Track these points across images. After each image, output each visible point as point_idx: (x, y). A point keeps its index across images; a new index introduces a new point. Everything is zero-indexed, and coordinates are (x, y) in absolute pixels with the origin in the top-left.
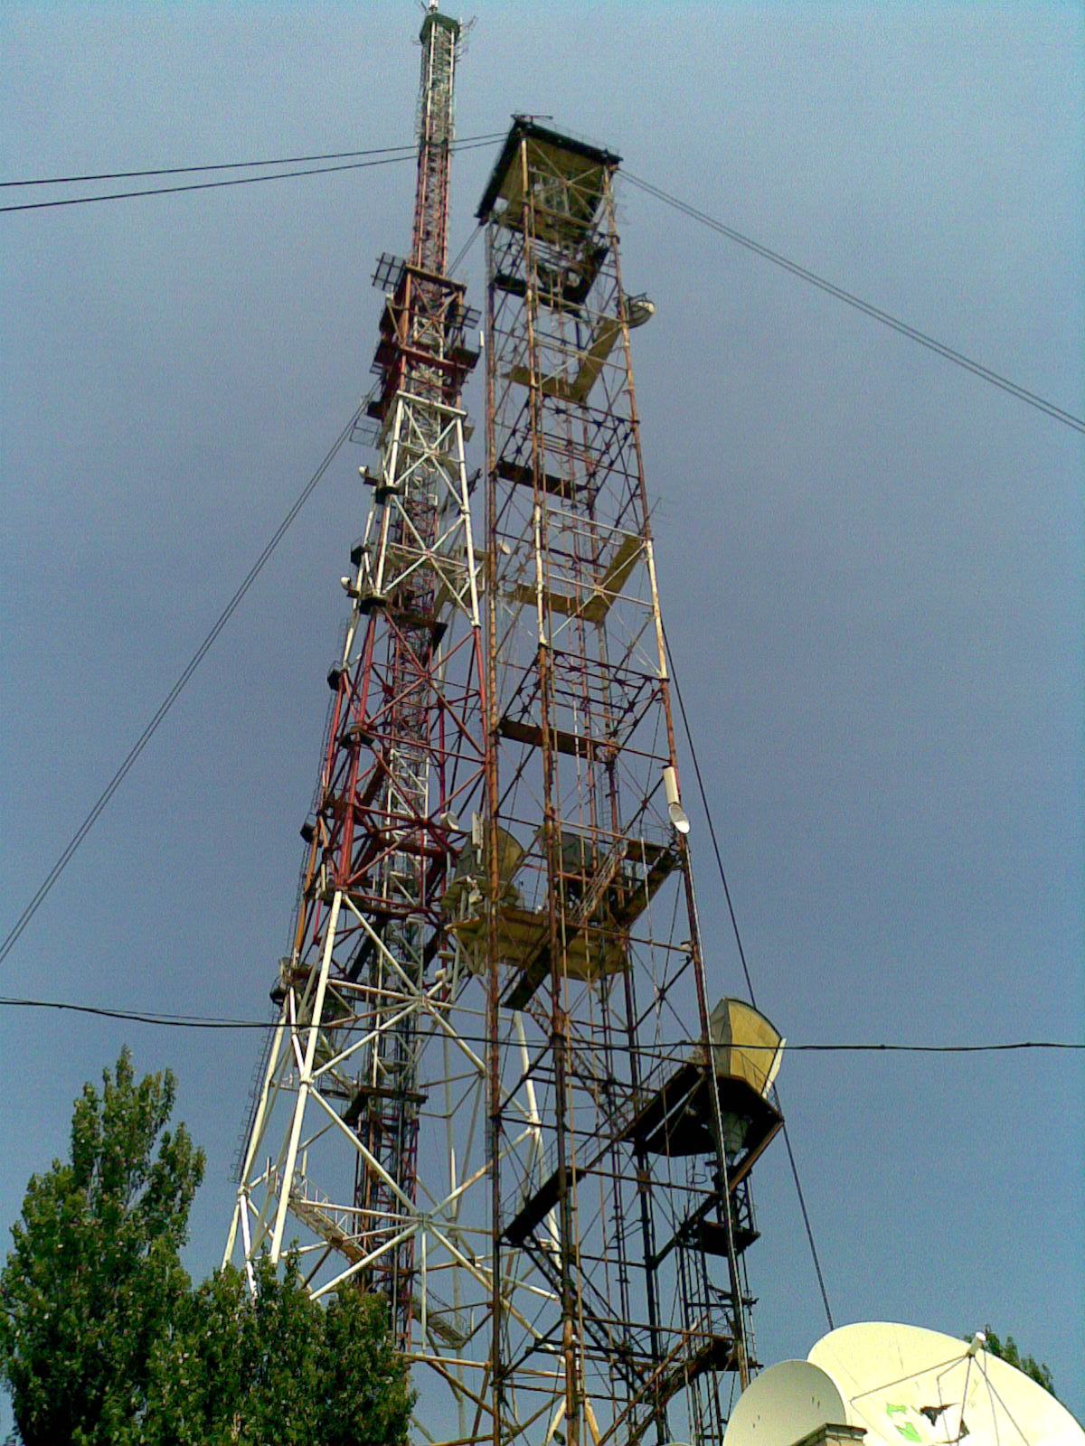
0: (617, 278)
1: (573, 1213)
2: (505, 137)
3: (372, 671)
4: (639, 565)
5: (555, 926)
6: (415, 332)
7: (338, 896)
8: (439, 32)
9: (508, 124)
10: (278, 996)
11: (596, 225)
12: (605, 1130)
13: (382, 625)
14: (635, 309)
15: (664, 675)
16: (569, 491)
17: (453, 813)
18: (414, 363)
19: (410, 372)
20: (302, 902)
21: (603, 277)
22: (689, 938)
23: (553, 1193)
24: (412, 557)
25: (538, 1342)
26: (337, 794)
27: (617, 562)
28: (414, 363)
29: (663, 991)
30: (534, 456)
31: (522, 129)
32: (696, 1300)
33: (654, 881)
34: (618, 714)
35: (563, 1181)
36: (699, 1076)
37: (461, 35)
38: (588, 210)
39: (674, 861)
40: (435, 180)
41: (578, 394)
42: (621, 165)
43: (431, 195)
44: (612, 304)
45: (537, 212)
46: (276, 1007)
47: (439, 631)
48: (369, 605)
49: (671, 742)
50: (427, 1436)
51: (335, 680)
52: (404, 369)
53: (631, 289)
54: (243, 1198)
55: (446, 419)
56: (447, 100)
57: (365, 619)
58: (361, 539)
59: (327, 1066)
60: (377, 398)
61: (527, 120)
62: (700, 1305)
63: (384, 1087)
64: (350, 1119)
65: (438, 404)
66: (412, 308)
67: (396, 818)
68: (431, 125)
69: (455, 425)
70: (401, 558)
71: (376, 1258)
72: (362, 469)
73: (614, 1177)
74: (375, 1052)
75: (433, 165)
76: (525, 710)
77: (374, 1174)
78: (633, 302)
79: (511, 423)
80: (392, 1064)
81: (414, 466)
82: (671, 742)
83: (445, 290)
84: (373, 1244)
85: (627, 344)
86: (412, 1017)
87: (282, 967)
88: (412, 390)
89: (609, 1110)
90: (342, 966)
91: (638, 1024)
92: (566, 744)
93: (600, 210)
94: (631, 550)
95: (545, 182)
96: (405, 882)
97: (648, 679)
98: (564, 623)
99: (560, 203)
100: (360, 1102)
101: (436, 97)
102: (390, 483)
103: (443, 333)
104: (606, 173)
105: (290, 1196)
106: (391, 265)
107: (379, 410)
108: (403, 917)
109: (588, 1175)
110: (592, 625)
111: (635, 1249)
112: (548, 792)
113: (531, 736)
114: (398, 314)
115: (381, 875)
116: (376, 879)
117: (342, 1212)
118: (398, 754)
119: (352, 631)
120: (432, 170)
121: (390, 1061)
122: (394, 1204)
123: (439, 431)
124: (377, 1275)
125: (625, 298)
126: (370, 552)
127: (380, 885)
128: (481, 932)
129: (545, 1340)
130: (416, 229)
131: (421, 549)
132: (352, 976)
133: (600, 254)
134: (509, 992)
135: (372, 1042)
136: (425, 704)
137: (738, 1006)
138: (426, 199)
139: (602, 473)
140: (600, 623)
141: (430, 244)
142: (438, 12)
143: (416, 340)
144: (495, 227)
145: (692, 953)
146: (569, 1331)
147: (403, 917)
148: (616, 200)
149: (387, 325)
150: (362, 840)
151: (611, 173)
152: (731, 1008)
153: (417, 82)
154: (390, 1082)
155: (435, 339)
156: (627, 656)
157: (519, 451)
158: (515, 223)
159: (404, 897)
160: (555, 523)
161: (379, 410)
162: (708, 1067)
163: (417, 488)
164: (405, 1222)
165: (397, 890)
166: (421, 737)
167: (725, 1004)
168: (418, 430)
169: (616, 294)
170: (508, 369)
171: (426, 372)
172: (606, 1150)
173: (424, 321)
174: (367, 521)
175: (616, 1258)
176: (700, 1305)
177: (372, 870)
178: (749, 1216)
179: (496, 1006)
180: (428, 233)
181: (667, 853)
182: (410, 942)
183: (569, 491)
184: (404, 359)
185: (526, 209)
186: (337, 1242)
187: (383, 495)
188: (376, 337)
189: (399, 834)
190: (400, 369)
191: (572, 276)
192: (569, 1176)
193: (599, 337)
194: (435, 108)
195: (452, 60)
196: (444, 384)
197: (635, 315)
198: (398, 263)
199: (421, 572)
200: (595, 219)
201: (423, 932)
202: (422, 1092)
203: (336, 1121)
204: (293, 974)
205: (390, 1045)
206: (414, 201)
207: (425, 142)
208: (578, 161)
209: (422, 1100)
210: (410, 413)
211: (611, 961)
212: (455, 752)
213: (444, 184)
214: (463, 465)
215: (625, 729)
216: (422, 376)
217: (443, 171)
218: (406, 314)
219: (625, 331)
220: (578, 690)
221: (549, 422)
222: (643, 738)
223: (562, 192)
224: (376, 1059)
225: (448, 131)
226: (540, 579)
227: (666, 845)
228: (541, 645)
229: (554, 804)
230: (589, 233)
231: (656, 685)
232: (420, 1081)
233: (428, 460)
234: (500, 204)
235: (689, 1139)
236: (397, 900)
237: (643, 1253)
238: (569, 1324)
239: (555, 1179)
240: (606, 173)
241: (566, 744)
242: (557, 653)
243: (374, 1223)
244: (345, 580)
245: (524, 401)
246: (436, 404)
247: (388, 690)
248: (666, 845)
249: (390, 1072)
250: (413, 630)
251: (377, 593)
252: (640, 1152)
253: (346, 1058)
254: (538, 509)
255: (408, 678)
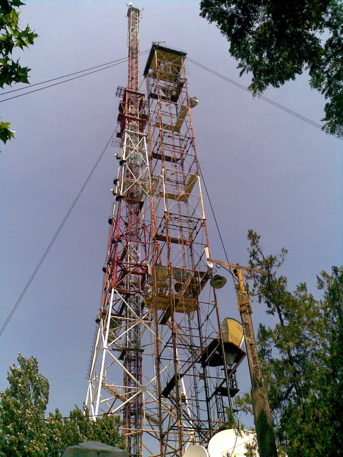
0: (186, 93)
1: (179, 388)
2: (150, 51)
3: (121, 219)
4: (196, 183)
5: (172, 300)
6: (131, 110)
7: (113, 290)
8: (133, 12)
9: (150, 47)
10: (98, 321)
11: (180, 76)
12: (191, 360)
13: (124, 203)
14: (192, 102)
15: (204, 218)
16: (175, 160)
17: (148, 262)
18: (130, 120)
19: (129, 123)
20: (104, 291)
21: (183, 93)
22: (214, 300)
23: (173, 383)
24: (132, 182)
25: (172, 427)
26: (113, 257)
27: (189, 183)
28: (130, 120)
29: (208, 316)
30: (162, 152)
31: (155, 47)
32: (220, 411)
33: (203, 283)
34: (191, 231)
35: (176, 377)
36: (218, 342)
37: (140, 13)
38: (177, 71)
39: (209, 276)
40: (134, 61)
41: (177, 129)
42: (187, 56)
43: (133, 66)
44: (186, 101)
45: (160, 74)
46: (98, 324)
47: (141, 204)
48: (119, 198)
49: (207, 239)
50: (151, 453)
51: (110, 222)
52: (127, 122)
53: (191, 96)
54: (90, 384)
55: (141, 137)
56: (137, 35)
57: (118, 202)
58: (116, 177)
59: (113, 341)
60: (119, 132)
61: (157, 44)
62: (221, 412)
63: (131, 348)
64: (121, 358)
65: (138, 133)
66: (128, 102)
67: (131, 264)
68: (132, 43)
69: (143, 139)
70: (128, 182)
71: (130, 400)
72: (116, 155)
73: (194, 376)
74: (128, 337)
75: (133, 56)
76: (163, 231)
77: (128, 375)
78: (192, 100)
79: (156, 141)
80: (133, 340)
81: (131, 153)
82: (207, 239)
83: (139, 96)
84: (130, 396)
85: (190, 113)
86: (138, 325)
87: (99, 312)
88: (130, 129)
89: (193, 353)
90: (117, 311)
91: (202, 326)
92: (175, 241)
93: (181, 70)
94: (193, 179)
95: (164, 63)
96: (134, 284)
97: (199, 220)
98: (173, 203)
99: (169, 69)
100: (124, 353)
101: (133, 34)
102: (124, 159)
103: (138, 110)
104: (182, 59)
105: (102, 384)
106: (121, 90)
107: (120, 135)
108: (134, 295)
109: (184, 376)
110: (184, 202)
111: (202, 396)
112: (169, 259)
113: (164, 239)
114: (124, 105)
115: (127, 282)
116: (126, 283)
117: (120, 388)
118: (130, 244)
119: (115, 206)
120: (133, 58)
121: (132, 339)
122: (135, 385)
123: (138, 140)
124: (132, 405)
125: (189, 98)
126: (119, 180)
127: (127, 285)
128: (152, 301)
129: (173, 426)
130: (129, 77)
131: (134, 179)
132: (120, 314)
133: (181, 85)
134: (161, 319)
135: (126, 333)
136: (138, 228)
137: (231, 320)
138: (131, 67)
139: (184, 155)
140: (186, 202)
141: (133, 81)
142: (132, 7)
143: (131, 112)
144: (149, 78)
145: (215, 304)
146: (179, 424)
147: (134, 295)
148: (185, 67)
149: (121, 109)
150: (120, 272)
151: (184, 59)
152: (228, 320)
153: (127, 29)
154: (133, 346)
155: (136, 112)
156: (194, 212)
157: (158, 150)
158: (154, 76)
159: (134, 288)
160: (169, 172)
161: (120, 135)
162: (220, 340)
163: (132, 159)
164: (138, 389)
165: (132, 286)
166: (138, 238)
167: (226, 319)
168: (132, 141)
169: (186, 98)
170: (155, 123)
171: (134, 123)
172: (190, 367)
173: (132, 106)
174: (119, 171)
175: (195, 399)
176: (221, 412)
177: (124, 280)
178: (236, 384)
179: (157, 324)
180: (132, 79)
181: (207, 274)
182: (137, 302)
183: (175, 160)
184: (126, 119)
185: (157, 73)
186: (118, 397)
187: (122, 163)
188: (118, 112)
189: (132, 269)
190: (125, 122)
191: (173, 92)
192: (178, 376)
193: (182, 112)
194: (133, 38)
195: (137, 22)
196: (140, 126)
197: (193, 104)
198: (123, 89)
199: (135, 186)
200: (180, 74)
201: (141, 298)
202: (142, 348)
203: (115, 361)
204: (102, 314)
205: (132, 335)
206: (128, 68)
207: (130, 48)
208: (173, 56)
209: (142, 351)
210: (129, 136)
211: (192, 307)
212: (148, 242)
213: (137, 63)
214: (146, 151)
215: (194, 235)
216: (132, 124)
217: (136, 58)
218: (126, 105)
219: (190, 110)
220: (179, 224)
221: (166, 140)
222: (198, 239)
223: (169, 66)
224: (128, 339)
225: (137, 45)
226: (164, 191)
227: (206, 272)
228: (165, 212)
229: (170, 261)
230: (178, 79)
231: (202, 221)
232: (142, 345)
233: (136, 150)
234: (150, 71)
235: (216, 361)
236: (132, 289)
237: (205, 397)
238: (179, 421)
239: (174, 378)
240: (182, 59)
241: (175, 241)
242: (170, 214)
243: (130, 390)
244: (112, 190)
245: (158, 135)
246: (137, 133)
247: (126, 224)
248: (206, 272)
249: (132, 343)
250: (133, 204)
251: (121, 194)
252: (204, 366)
253: (120, 338)
254: (163, 169)
255: (132, 220)
